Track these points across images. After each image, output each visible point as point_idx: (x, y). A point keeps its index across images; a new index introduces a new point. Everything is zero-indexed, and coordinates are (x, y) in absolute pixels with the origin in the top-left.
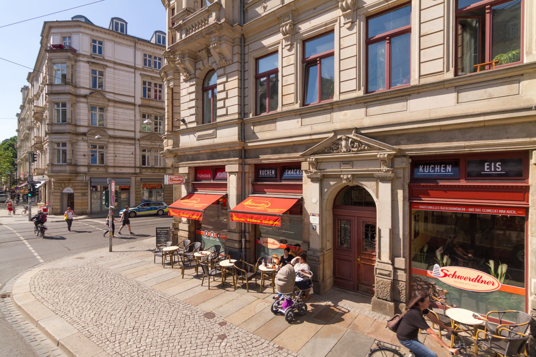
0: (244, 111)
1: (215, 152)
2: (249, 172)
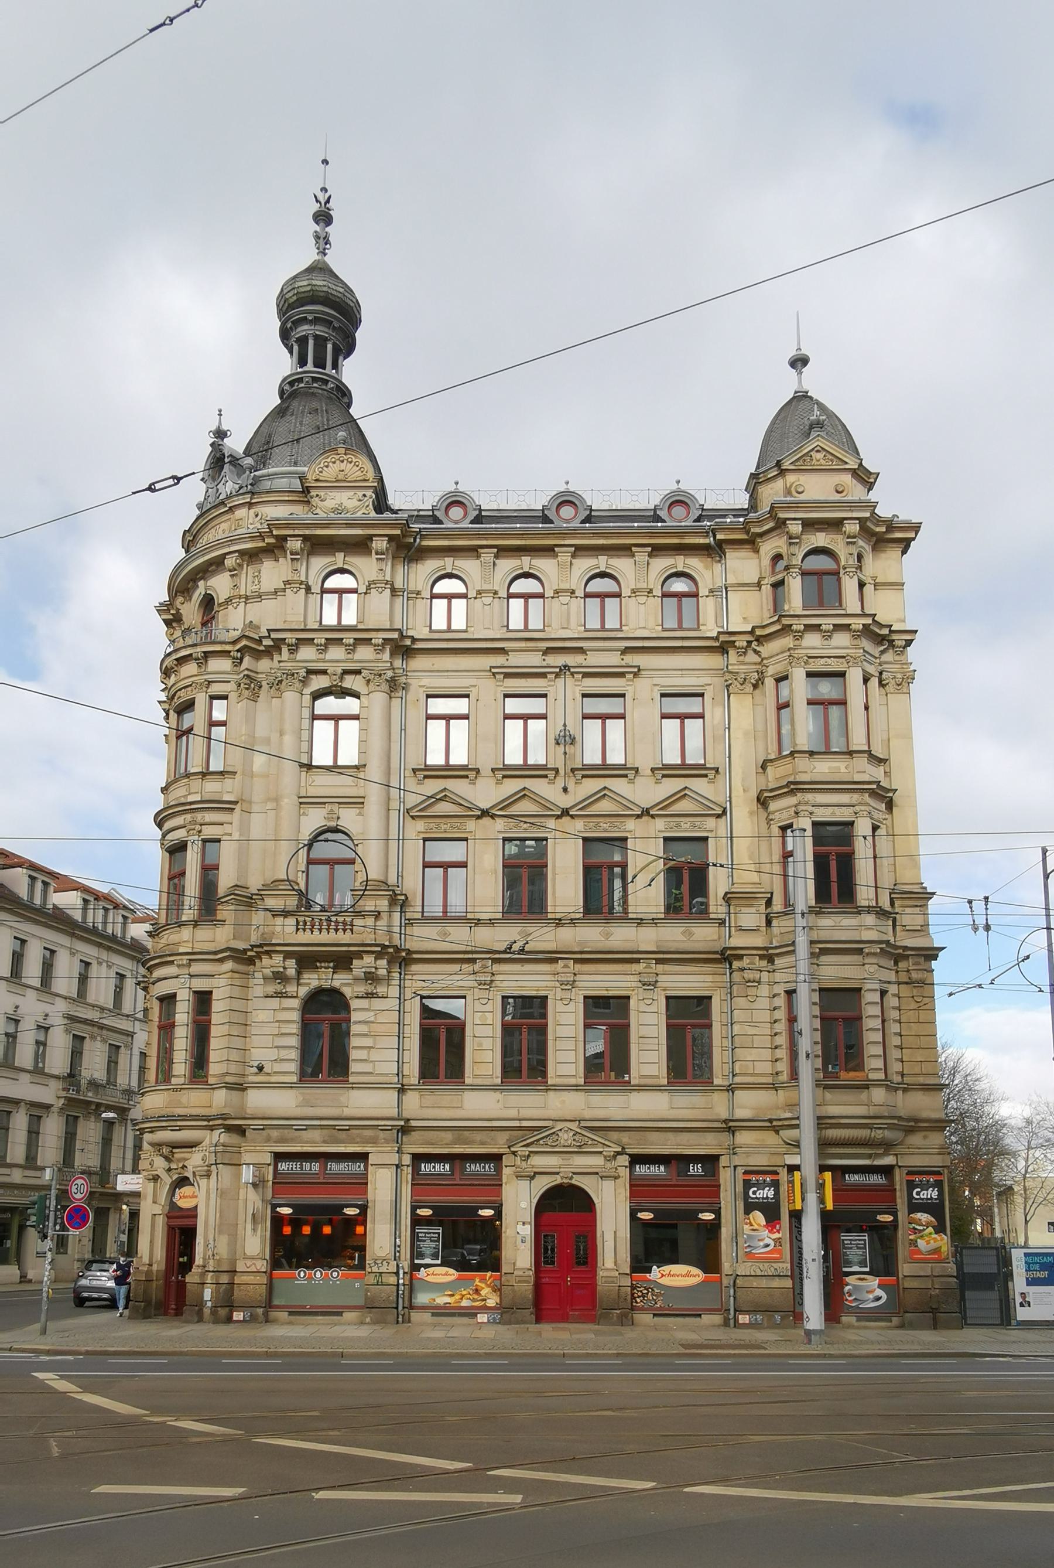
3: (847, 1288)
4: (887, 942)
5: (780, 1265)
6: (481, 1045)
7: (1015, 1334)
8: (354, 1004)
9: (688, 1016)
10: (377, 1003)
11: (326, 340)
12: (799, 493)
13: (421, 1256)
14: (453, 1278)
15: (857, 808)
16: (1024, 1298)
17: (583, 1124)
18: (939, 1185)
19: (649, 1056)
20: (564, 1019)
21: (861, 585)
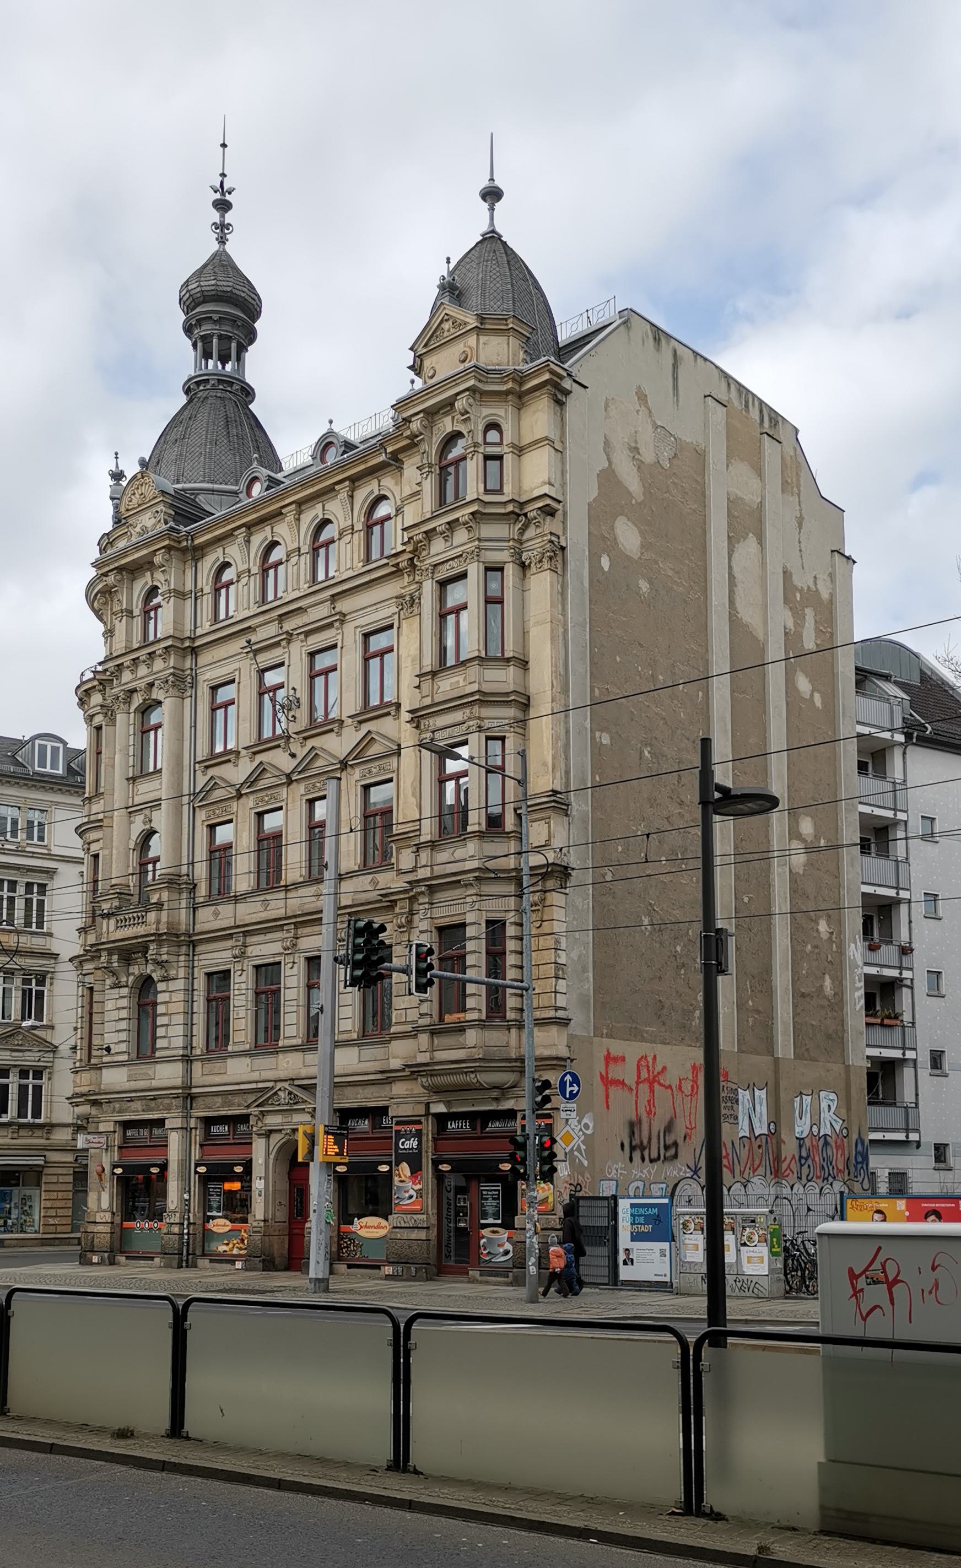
0: (191, 1044)
1: (153, 1097)
2: (196, 1128)
3: (483, 1241)
5: (419, 1216)
7: (624, 1295)
13: (210, 1209)
14: (227, 1229)
16: (628, 1255)
17: (296, 1082)
18: (419, 1134)
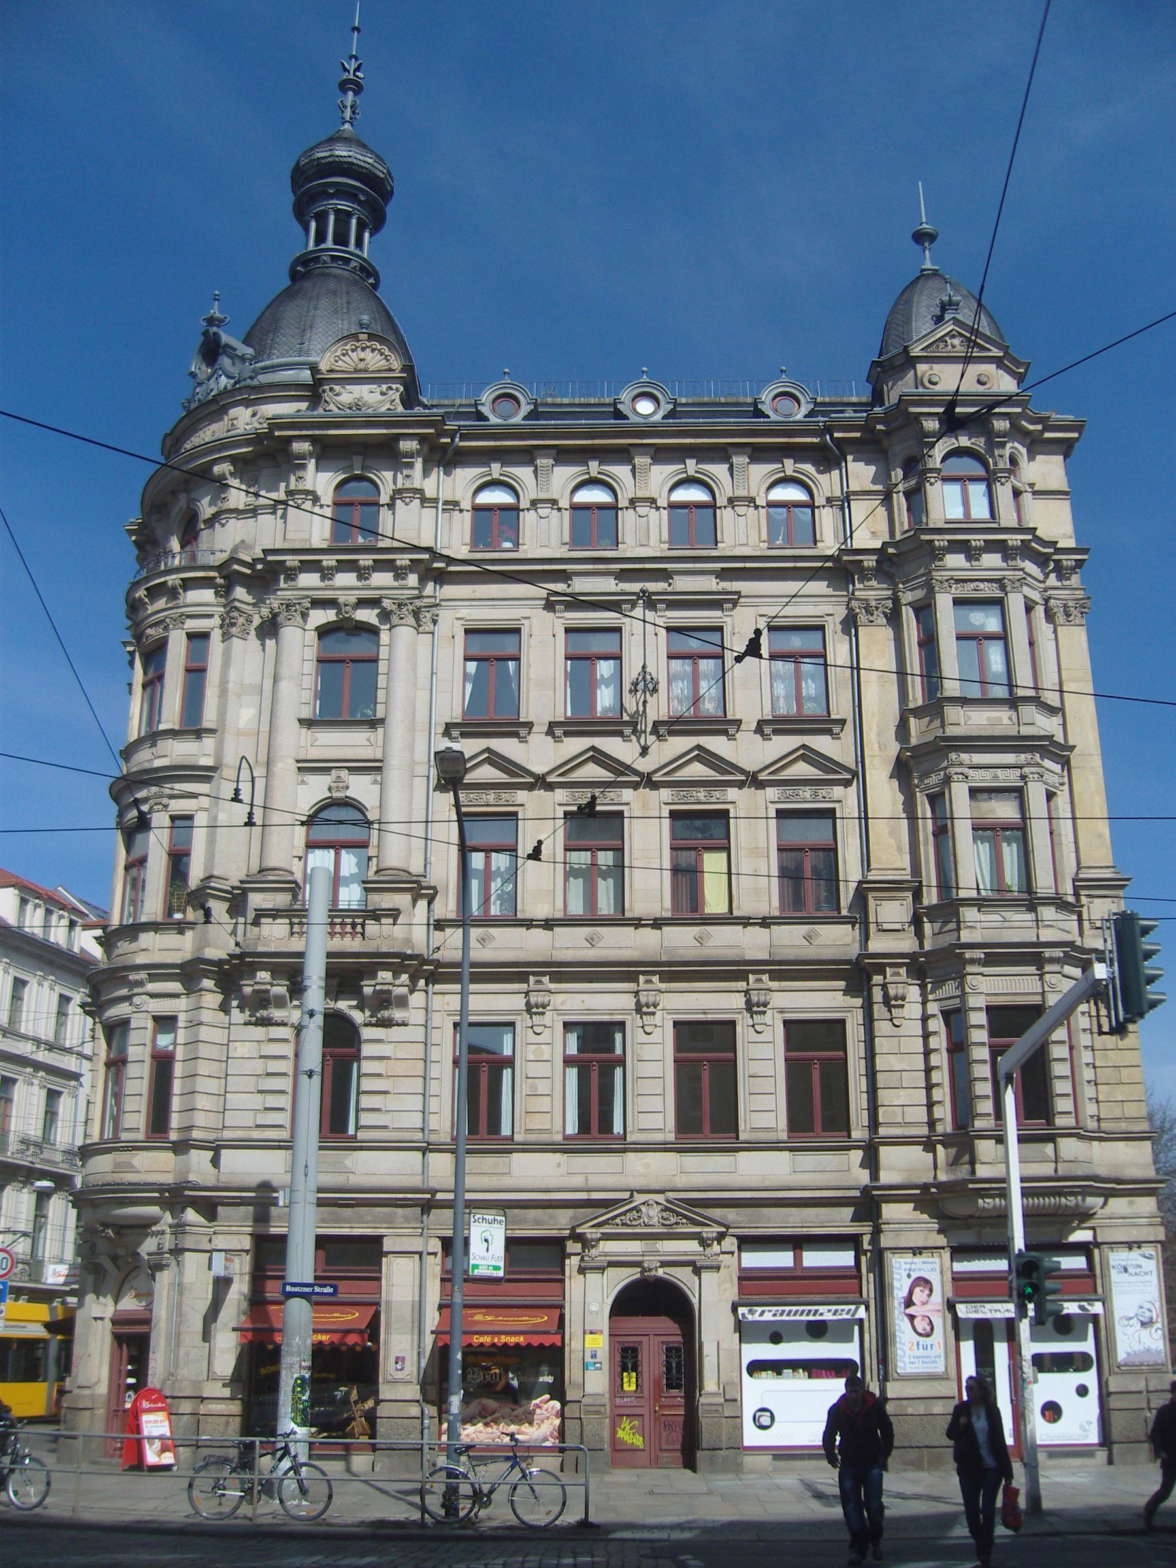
4: (1071, 944)
6: (534, 1087)
8: (367, 1033)
9: (814, 1049)
10: (395, 1033)
11: (349, 215)
12: (935, 384)
15: (1026, 770)
17: (671, 1195)
19: (763, 1101)
20: (647, 1052)
21: (1017, 493)
